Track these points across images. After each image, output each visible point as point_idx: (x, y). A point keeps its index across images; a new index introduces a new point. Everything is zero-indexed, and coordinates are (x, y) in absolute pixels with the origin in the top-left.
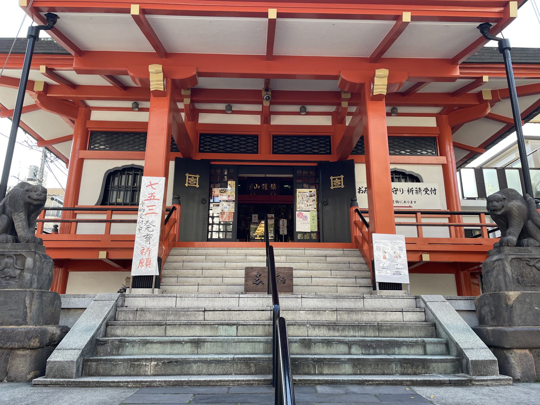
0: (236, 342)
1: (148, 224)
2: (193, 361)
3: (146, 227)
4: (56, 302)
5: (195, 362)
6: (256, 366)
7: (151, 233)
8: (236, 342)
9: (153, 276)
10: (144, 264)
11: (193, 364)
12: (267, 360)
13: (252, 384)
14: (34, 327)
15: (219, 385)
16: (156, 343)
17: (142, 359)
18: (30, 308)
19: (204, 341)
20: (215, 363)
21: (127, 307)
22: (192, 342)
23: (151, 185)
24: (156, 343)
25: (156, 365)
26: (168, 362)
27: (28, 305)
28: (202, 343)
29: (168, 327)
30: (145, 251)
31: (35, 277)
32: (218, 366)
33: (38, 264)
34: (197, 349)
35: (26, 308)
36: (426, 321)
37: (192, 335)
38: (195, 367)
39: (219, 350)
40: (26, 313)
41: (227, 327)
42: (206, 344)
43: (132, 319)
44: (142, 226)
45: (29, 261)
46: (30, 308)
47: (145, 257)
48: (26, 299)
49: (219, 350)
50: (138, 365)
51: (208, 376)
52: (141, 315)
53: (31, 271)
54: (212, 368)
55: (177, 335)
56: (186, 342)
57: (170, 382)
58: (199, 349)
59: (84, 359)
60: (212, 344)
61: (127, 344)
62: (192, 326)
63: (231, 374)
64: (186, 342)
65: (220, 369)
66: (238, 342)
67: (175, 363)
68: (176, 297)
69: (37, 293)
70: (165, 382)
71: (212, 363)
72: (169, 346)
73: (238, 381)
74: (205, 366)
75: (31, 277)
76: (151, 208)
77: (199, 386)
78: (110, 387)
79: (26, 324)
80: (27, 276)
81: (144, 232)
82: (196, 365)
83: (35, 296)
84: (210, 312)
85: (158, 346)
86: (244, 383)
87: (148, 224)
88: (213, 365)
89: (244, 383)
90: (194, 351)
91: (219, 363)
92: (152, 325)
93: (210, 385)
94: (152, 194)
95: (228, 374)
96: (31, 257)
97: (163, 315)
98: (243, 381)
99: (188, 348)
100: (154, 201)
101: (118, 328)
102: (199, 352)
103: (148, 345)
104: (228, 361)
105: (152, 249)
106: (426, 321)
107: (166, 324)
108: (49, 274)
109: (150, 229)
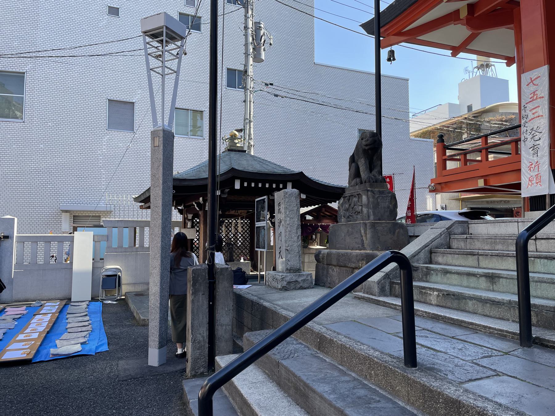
0: (536, 282)
1: (533, 132)
2: (468, 297)
3: (531, 136)
4: (397, 231)
5: (471, 298)
6: (537, 316)
7: (538, 142)
8: (536, 282)
9: (545, 195)
10: (534, 182)
11: (468, 300)
12: (553, 310)
13: (505, 336)
14: (371, 252)
15: (471, 328)
16: (454, 273)
17: (427, 288)
18: (366, 236)
19: (499, 277)
20: (490, 303)
21: (471, 234)
22: (486, 276)
23: (532, 81)
24: (454, 273)
25: (438, 296)
26: (447, 295)
27: (363, 234)
28: (496, 279)
29: (480, 257)
30: (533, 166)
31: (371, 211)
32: (493, 307)
33: (371, 199)
34: (493, 285)
35: (362, 236)
36: (412, 217)
37: (506, 268)
38: (470, 303)
39: (465, 283)
40: (362, 240)
41: (546, 261)
42: (501, 280)
43: (463, 247)
44: (527, 136)
45: (364, 198)
46: (366, 236)
47: (534, 174)
48: (362, 229)
49: (465, 283)
50: (425, 293)
51: (485, 319)
52: (470, 243)
53: (367, 206)
54: (487, 309)
55: (490, 266)
56: (481, 276)
57: (429, 313)
58: (494, 286)
59: (391, 281)
60: (508, 280)
61: (432, 272)
62: (505, 258)
63: (508, 320)
64: (481, 276)
65: (495, 312)
66: (539, 282)
67: (452, 297)
68: (518, 222)
69: (369, 224)
70: (426, 312)
71: (487, 303)
72: (465, 277)
73: (490, 328)
74: (480, 305)
75: (368, 211)
76: (534, 111)
77: (453, 324)
78: (391, 308)
79: (365, 249)
80: (365, 210)
81: (530, 143)
82: (471, 302)
83: (368, 227)
84: (543, 241)
85: (456, 276)
86: (496, 332)
87: (533, 132)
88: (488, 305)
89: (496, 332)
90: (489, 287)
91: (494, 304)
92: (466, 254)
93: (469, 328)
94: (534, 92)
95: (505, 320)
96: (365, 195)
97: (491, 243)
98: (495, 329)
99: (483, 282)
100: (539, 100)
101: (439, 256)
102: (495, 289)
103: (448, 275)
104: (504, 304)
105: (541, 163)
106: (412, 217)
107: (478, 254)
108: (388, 207)
109: (537, 138)
